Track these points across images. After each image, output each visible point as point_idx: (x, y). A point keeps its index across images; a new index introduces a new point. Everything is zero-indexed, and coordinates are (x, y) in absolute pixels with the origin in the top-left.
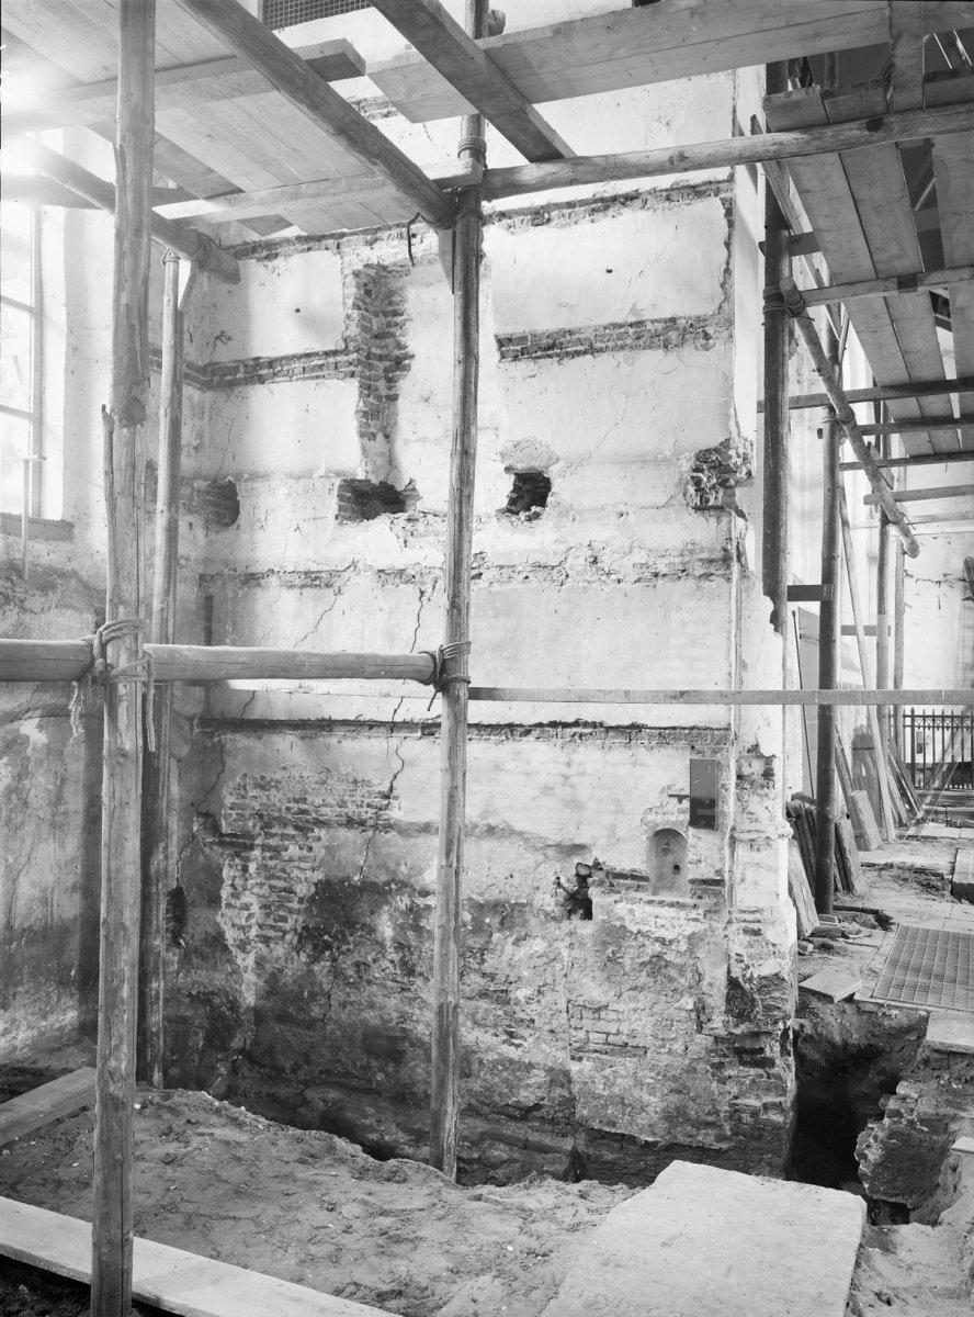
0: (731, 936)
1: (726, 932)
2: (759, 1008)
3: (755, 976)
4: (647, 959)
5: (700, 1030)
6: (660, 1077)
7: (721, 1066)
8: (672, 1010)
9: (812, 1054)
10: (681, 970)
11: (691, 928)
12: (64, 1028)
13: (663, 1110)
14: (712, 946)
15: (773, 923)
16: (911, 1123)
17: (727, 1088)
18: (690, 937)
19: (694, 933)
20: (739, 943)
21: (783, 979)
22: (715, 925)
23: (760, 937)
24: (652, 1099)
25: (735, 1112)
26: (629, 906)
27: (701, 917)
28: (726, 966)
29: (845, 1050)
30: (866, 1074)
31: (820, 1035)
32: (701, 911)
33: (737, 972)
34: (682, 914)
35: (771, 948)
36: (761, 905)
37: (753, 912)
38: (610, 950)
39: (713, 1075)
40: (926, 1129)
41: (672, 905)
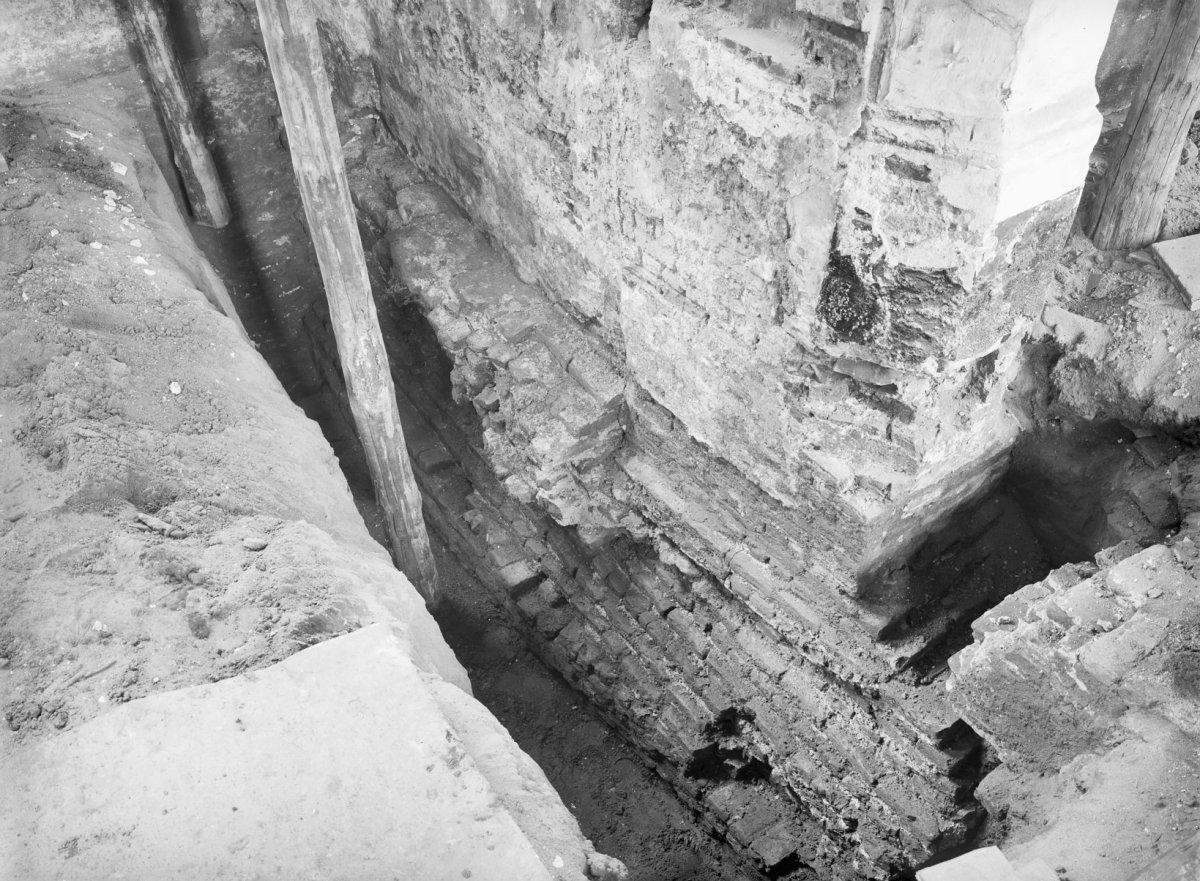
0: (852, 168)
1: (845, 158)
2: (884, 327)
3: (892, 262)
4: (716, 161)
5: (779, 320)
6: (718, 364)
7: (803, 390)
8: (742, 270)
9: (1075, 393)
10: (762, 201)
11: (789, 126)
12: (104, 49)
13: (719, 411)
14: (814, 179)
15: (965, 162)
16: (1061, 662)
17: (803, 428)
18: (783, 145)
19: (788, 139)
20: (868, 186)
21: (958, 287)
22: (829, 133)
23: (925, 185)
24: (706, 388)
25: (804, 467)
26: (701, 41)
27: (806, 107)
28: (831, 228)
29: (1144, 409)
30: (1165, 463)
31: (1109, 366)
32: (807, 94)
33: (851, 245)
34: (778, 88)
35: (949, 216)
36: (951, 110)
37: (924, 124)
38: (667, 123)
39: (786, 399)
40: (1082, 687)
41: (763, 63)
